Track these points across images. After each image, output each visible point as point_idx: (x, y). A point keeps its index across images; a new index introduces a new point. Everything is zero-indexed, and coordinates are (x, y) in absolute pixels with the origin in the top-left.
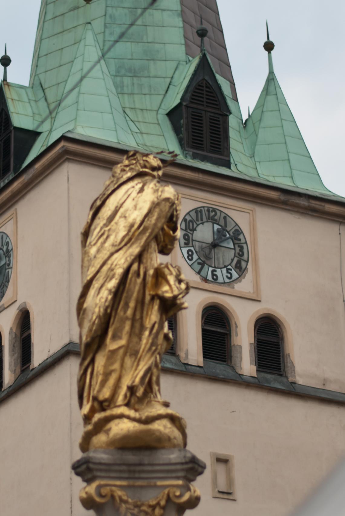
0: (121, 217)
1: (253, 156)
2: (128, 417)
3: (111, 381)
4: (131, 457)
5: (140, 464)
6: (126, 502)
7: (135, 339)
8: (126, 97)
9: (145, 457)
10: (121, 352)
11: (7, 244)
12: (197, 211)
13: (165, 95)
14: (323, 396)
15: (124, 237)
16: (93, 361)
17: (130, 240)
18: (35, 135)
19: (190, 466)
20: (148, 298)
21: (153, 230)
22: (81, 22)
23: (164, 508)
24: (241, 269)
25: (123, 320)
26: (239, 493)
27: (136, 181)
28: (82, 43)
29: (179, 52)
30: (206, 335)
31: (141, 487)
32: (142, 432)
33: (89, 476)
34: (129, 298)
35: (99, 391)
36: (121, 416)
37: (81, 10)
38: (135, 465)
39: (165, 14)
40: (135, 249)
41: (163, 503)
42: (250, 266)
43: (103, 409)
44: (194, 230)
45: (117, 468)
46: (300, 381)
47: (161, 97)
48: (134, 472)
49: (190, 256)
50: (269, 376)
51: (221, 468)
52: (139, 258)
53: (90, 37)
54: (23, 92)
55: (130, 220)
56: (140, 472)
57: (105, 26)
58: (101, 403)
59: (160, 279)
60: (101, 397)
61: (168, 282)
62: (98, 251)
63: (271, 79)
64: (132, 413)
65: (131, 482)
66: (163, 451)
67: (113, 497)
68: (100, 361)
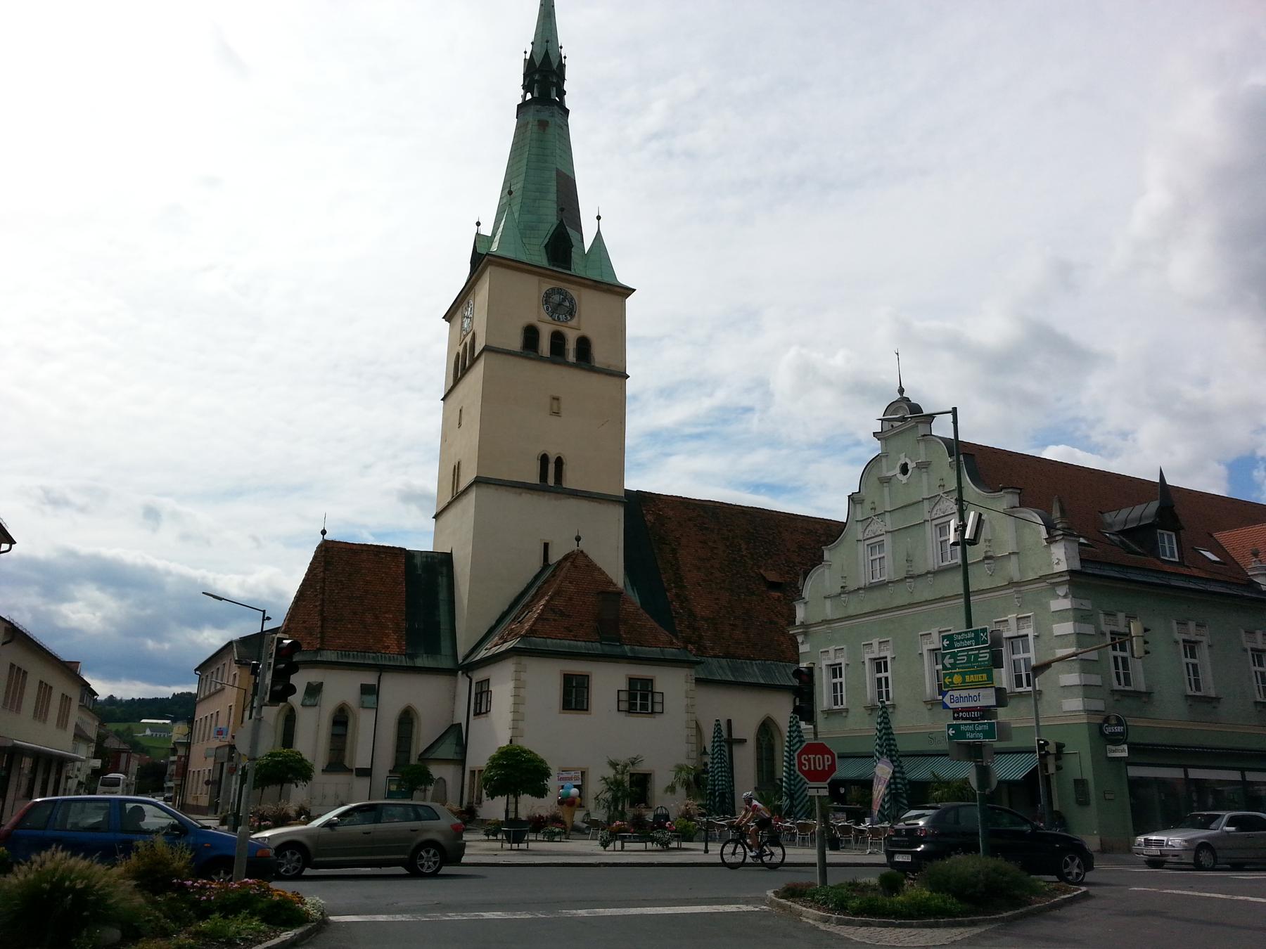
12: (553, 289)
24: (572, 315)
42: (576, 315)
49: (547, 309)
51: (555, 402)
63: (599, 232)
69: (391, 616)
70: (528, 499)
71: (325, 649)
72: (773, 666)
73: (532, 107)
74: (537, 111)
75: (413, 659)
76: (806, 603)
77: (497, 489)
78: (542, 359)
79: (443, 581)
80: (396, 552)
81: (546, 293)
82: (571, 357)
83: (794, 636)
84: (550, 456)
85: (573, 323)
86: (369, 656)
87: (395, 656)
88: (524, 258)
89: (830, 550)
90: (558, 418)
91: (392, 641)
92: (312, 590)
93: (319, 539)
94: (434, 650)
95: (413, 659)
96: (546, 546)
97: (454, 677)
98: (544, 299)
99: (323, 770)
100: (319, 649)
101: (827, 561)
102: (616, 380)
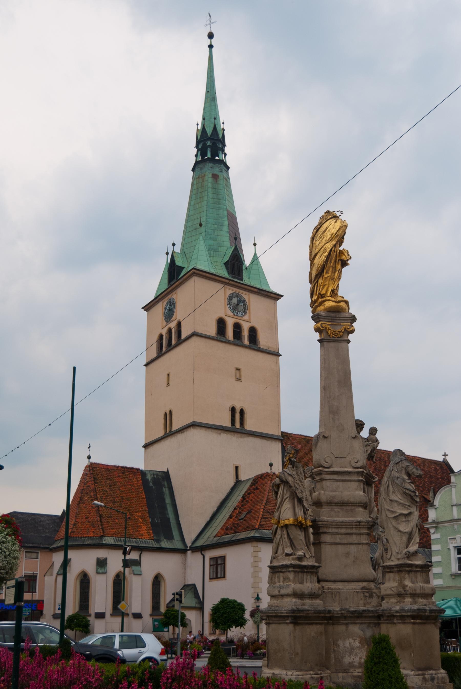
0: (328, 231)
1: (249, 278)
2: (332, 301)
3: (325, 288)
4: (332, 315)
5: (336, 317)
6: (330, 330)
7: (333, 274)
8: (211, 257)
9: (337, 315)
10: (329, 278)
11: (174, 301)
12: (233, 294)
13: (223, 258)
14: (268, 352)
15: (329, 238)
16: (317, 282)
17: (332, 239)
18: (183, 268)
19: (353, 318)
20: (337, 260)
21: (340, 236)
22: (197, 233)
23: (343, 332)
24: (245, 313)
25: (329, 267)
26: (243, 379)
27: (333, 219)
28: (199, 240)
29: (228, 244)
30: (234, 332)
31: (335, 325)
32: (336, 306)
33: (318, 320)
34: (331, 259)
35: (321, 291)
36: (329, 300)
37: (198, 230)
38: (334, 317)
39: (224, 232)
40: (334, 242)
41: (343, 331)
42: (248, 312)
43: (322, 298)
44: (232, 299)
45: (327, 318)
46: (262, 347)
47: (222, 258)
48: (333, 319)
49: (230, 307)
50: (252, 345)
51: (238, 372)
52: (335, 246)
53: (201, 238)
54: (179, 254)
55: (332, 232)
56: (335, 320)
57: (205, 235)
58: (322, 295)
59: (341, 254)
60: (322, 293)
61: (344, 255)
62: (320, 243)
64: (333, 299)
65: (332, 323)
66: (343, 313)
67: (326, 328)
68: (320, 281)
69: (140, 514)
70: (225, 437)
71: (106, 536)
72: (374, 546)
73: (208, 164)
74: (211, 168)
75: (159, 543)
76: (436, 509)
77: (206, 430)
78: (228, 342)
79: (166, 491)
80: (134, 471)
81: (229, 296)
82: (246, 341)
83: (428, 529)
84: (236, 408)
85: (246, 317)
86: (121, 540)
87: (148, 540)
88: (213, 271)
89: (455, 476)
90: (240, 382)
91: (144, 529)
92: (88, 496)
93: (86, 462)
94: (170, 537)
95: (159, 543)
96: (237, 468)
97: (184, 555)
98: (228, 300)
99: (111, 614)
100: (103, 536)
101: (454, 483)
102: (274, 358)
